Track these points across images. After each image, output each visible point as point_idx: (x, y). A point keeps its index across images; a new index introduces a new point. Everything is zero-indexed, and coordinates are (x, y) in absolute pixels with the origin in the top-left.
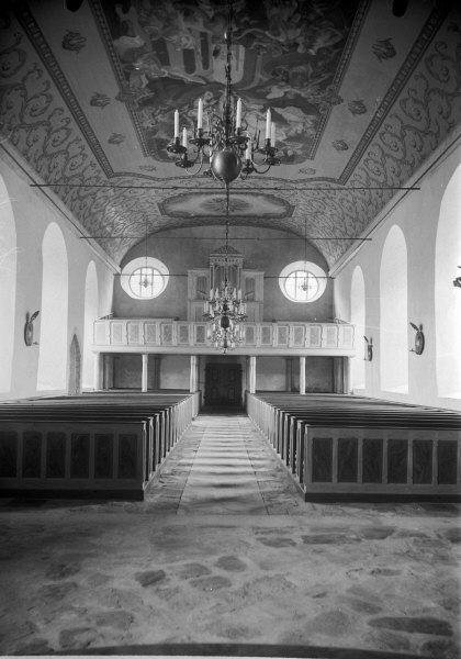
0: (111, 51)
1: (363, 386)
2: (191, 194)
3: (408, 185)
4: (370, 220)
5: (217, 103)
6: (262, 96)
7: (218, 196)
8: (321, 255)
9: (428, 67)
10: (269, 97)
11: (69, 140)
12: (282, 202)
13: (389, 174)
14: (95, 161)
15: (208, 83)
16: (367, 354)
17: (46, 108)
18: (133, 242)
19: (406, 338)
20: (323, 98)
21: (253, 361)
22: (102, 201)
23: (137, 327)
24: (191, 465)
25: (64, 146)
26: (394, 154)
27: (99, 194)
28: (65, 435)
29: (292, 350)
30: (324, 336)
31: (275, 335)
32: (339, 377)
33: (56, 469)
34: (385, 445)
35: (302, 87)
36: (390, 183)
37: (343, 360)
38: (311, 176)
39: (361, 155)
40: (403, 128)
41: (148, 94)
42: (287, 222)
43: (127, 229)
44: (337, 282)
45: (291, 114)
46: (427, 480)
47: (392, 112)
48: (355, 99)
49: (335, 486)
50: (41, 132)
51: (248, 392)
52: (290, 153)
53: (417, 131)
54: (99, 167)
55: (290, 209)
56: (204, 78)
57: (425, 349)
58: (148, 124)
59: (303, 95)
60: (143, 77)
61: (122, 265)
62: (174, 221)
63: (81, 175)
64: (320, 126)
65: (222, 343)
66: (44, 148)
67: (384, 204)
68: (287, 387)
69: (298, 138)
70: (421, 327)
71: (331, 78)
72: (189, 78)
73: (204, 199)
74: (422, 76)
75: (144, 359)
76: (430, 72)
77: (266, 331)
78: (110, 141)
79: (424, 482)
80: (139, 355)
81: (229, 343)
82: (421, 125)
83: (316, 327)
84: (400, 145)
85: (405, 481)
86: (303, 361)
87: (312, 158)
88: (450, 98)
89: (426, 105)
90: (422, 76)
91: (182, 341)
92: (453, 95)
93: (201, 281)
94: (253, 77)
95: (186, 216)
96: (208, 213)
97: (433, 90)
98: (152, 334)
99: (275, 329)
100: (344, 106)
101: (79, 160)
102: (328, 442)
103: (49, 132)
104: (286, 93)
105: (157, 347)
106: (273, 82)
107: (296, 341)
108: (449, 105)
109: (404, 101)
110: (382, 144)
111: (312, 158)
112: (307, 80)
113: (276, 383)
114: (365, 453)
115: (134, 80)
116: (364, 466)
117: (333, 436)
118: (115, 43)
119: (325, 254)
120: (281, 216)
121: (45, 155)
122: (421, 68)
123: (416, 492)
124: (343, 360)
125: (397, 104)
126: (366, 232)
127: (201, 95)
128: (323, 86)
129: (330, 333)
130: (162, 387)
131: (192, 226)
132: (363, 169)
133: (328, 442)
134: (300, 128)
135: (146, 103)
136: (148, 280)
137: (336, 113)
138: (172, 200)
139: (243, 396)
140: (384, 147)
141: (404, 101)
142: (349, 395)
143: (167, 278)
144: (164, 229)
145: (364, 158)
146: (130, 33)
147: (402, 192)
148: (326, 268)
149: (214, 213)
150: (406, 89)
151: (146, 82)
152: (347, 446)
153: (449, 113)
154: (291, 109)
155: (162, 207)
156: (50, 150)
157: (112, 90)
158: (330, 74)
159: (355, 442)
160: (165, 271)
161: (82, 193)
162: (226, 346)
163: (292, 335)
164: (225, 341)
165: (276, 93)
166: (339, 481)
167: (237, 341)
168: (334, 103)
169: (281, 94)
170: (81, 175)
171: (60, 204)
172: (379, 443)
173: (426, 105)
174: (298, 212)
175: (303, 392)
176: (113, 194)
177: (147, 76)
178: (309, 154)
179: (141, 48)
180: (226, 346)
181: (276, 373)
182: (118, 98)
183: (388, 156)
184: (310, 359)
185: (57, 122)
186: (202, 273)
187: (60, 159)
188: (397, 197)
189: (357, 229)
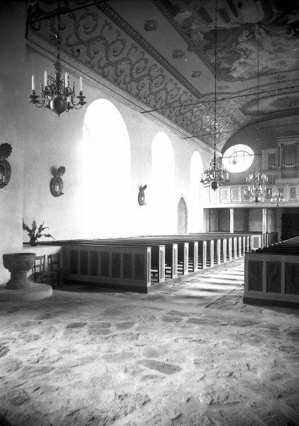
0: (174, 24)
6: (284, 23)
7: (280, 97)
11: (165, 81)
14: (186, 90)
15: (242, 25)
17: (146, 67)
18: (229, 136)
21: (264, 212)
22: (198, 113)
23: (226, 192)
25: (163, 86)
27: (195, 110)
28: (109, 253)
33: (84, 272)
41: (206, 43)
43: (225, 130)
46: (259, 288)
49: (263, 294)
50: (146, 81)
54: (190, 93)
56: (238, 23)
58: (213, 60)
60: (199, 33)
61: (223, 152)
62: (256, 118)
63: (179, 100)
65: (254, 199)
66: (150, 90)
72: (228, 26)
75: (232, 212)
78: (193, 76)
80: (228, 209)
81: (259, 199)
94: (272, 13)
96: (276, 109)
98: (236, 195)
101: (175, 91)
103: (151, 79)
105: (239, 203)
115: (194, 37)
118: (175, 18)
121: (151, 93)
127: (240, 34)
130: (250, 230)
135: (207, 48)
136: (240, 158)
138: (248, 104)
143: (253, 157)
144: (249, 125)
146: (181, 10)
149: (283, 108)
151: (202, 36)
155: (243, 110)
156: (154, 90)
157: (183, 46)
159: (279, 264)
160: (252, 152)
161: (182, 111)
162: (257, 201)
164: (257, 198)
170: (179, 100)
171: (161, 117)
176: (204, 108)
177: (201, 32)
179: (191, 17)
180: (257, 201)
182: (189, 50)
185: (154, 73)
186: (272, 151)
187: (163, 94)
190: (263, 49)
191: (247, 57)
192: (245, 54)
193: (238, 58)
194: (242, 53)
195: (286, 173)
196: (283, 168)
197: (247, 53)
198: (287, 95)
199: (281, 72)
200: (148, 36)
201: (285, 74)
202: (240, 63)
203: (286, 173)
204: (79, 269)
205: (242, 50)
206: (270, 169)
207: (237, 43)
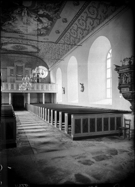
1: (61, 101)
2: (9, 43)
3: (79, 44)
5: (22, 13)
8: (47, 65)
10: (39, 13)
16: (63, 92)
19: (77, 88)
24: (23, 129)
26: (74, 35)
29: (40, 91)
31: (40, 87)
32: (53, 99)
35: (49, 11)
36: (71, 44)
37: (54, 94)
38: (47, 41)
39: (62, 36)
40: (78, 28)
44: (51, 73)
45: (44, 20)
51: (27, 104)
52: (42, 33)
53: (82, 29)
59: (49, 14)
64: (52, 25)
65: (26, 89)
69: (45, 28)
70: (83, 84)
71: (59, 10)
73: (12, 45)
74: (86, 13)
76: (89, 11)
77: (12, 85)
79: (106, 130)
80: (42, 93)
82: (84, 27)
83: (47, 84)
84: (76, 33)
85: (101, 131)
86: (44, 94)
90: (86, 13)
91: (12, 88)
92: (95, 19)
93: (12, 70)
95: (6, 50)
97: (89, 17)
99: (40, 85)
100: (61, 19)
102: (80, 120)
104: (44, 13)
106: (41, 8)
108: (93, 21)
109: (79, 20)
110: (70, 32)
112: (51, 9)
114: (90, 122)
116: (90, 127)
120: (35, 53)
122: (86, 10)
124: (54, 94)
128: (56, 12)
131: (7, 53)
133: (80, 120)
134: (46, 25)
139: (25, 105)
141: (79, 20)
145: (64, 36)
148: (48, 69)
149: (16, 50)
150: (80, 16)
154: (45, 18)
158: (58, 8)
159: (87, 119)
162: (27, 90)
163: (45, 87)
164: (27, 88)
165: (41, 12)
166: (90, 132)
167: (22, 88)
168: (58, 18)
169: (43, 13)
172: (94, 119)
174: (41, 52)
175: (44, 103)
178: (47, 34)
183: (72, 36)
184: (45, 93)
186: (12, 68)
188: (74, 48)
189: (58, 57)
192: (13, 20)
193: (9, 20)
197: (15, 20)
198: (20, 45)
200: (108, 8)
202: (8, 23)
203: (18, 78)
205: (13, 17)
207: (13, 13)
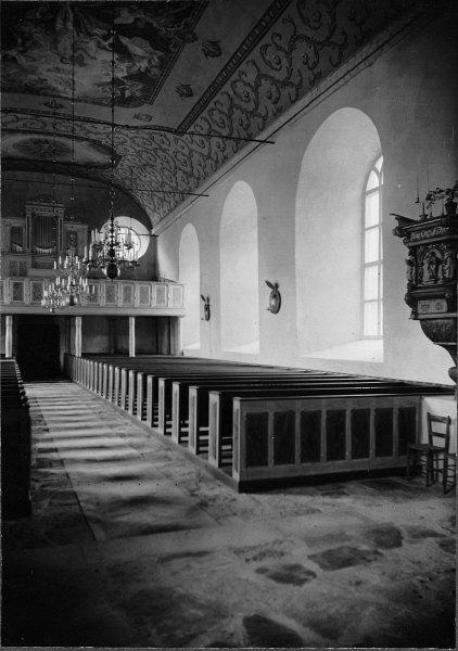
1: (197, 346)
3: (262, 137)
4: (207, 175)
8: (144, 212)
9: (299, 9)
12: (111, 151)
13: (236, 125)
16: (204, 314)
19: (258, 299)
20: (176, 33)
21: (78, 322)
29: (119, 307)
30: (155, 295)
34: (324, 417)
35: (156, 15)
36: (235, 135)
38: (148, 123)
42: (107, 173)
45: (137, 48)
46: (389, 453)
47: (249, 58)
48: (211, 39)
55: (116, 157)
57: (282, 306)
59: (155, 25)
64: (166, 65)
65: (68, 300)
67: (226, 158)
68: (110, 348)
76: (300, 14)
80: (126, 318)
81: (76, 300)
87: (151, 103)
88: (318, 47)
89: (288, 54)
92: (323, 44)
96: (20, 155)
102: (263, 417)
107: (125, 300)
108: (316, 54)
111: (151, 103)
113: (99, 344)
116: (302, 443)
117: (269, 411)
119: (148, 211)
123: (357, 469)
125: (258, 48)
126: (205, 187)
129: (160, 292)
132: (206, 120)
133: (263, 417)
134: (144, 65)
137: (190, 53)
140: (234, 97)
141: (266, 46)
142: (178, 355)
147: (254, 144)
148: (149, 226)
149: (31, 157)
152: (284, 421)
153: (316, 64)
159: (292, 414)
162: (72, 303)
164: (72, 298)
168: (189, 41)
169: (131, 21)
173: (288, 54)
174: (125, 163)
178: (147, 97)
181: (98, 334)
184: (139, 319)
186: (16, 222)
190: (56, 48)
191: (23, 52)
194: (20, 40)
195: (39, 260)
196: (34, 254)
197: (28, 44)
198: (47, 137)
199: (60, 97)
201: (64, 103)
203: (39, 260)
204: (380, 550)
206: (12, 251)
